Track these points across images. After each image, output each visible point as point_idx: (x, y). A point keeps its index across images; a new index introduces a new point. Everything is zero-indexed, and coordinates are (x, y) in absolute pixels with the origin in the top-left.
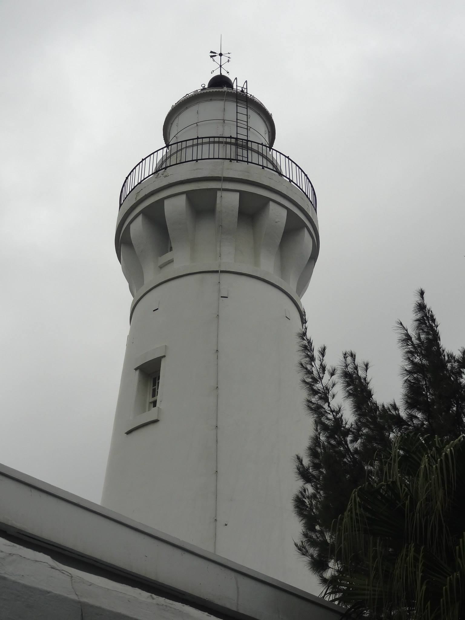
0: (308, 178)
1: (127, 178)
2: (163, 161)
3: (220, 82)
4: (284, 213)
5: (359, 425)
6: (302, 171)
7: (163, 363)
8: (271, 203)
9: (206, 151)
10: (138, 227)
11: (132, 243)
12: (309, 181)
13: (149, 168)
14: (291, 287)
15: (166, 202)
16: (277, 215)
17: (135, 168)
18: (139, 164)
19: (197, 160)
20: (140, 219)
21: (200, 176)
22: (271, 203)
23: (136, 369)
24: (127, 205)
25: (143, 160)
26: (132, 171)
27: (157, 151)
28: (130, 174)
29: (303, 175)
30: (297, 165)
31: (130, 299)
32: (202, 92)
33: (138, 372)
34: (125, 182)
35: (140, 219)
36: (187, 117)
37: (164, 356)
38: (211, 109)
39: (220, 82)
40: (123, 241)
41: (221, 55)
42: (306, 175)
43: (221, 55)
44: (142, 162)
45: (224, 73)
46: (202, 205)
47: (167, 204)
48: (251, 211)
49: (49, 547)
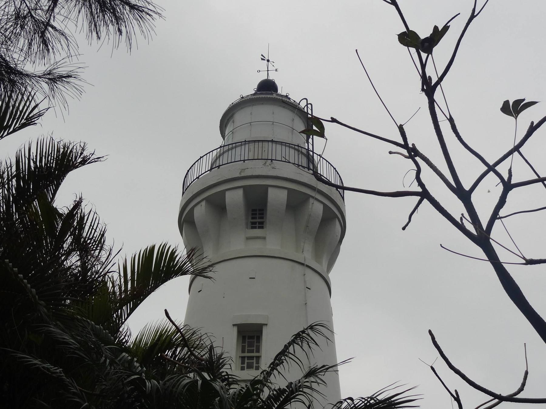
0: (336, 171)
1: (188, 171)
2: (218, 157)
3: (267, 87)
5: (131, 290)
6: (331, 165)
7: (265, 330)
9: (279, 152)
10: (200, 211)
11: (194, 222)
12: (338, 173)
13: (205, 165)
14: (321, 268)
17: (195, 163)
18: (198, 161)
19: (244, 161)
20: (203, 203)
21: (302, 181)
23: (234, 325)
24: (189, 195)
25: (201, 157)
26: (193, 166)
27: (212, 151)
28: (191, 168)
29: (332, 168)
30: (327, 161)
32: (253, 97)
33: (235, 329)
34: (187, 174)
35: (203, 203)
37: (266, 325)
38: (264, 112)
39: (267, 87)
41: (268, 61)
42: (335, 169)
43: (268, 61)
44: (200, 159)
45: (271, 78)
46: (218, 205)
47: (228, 195)
48: (296, 203)
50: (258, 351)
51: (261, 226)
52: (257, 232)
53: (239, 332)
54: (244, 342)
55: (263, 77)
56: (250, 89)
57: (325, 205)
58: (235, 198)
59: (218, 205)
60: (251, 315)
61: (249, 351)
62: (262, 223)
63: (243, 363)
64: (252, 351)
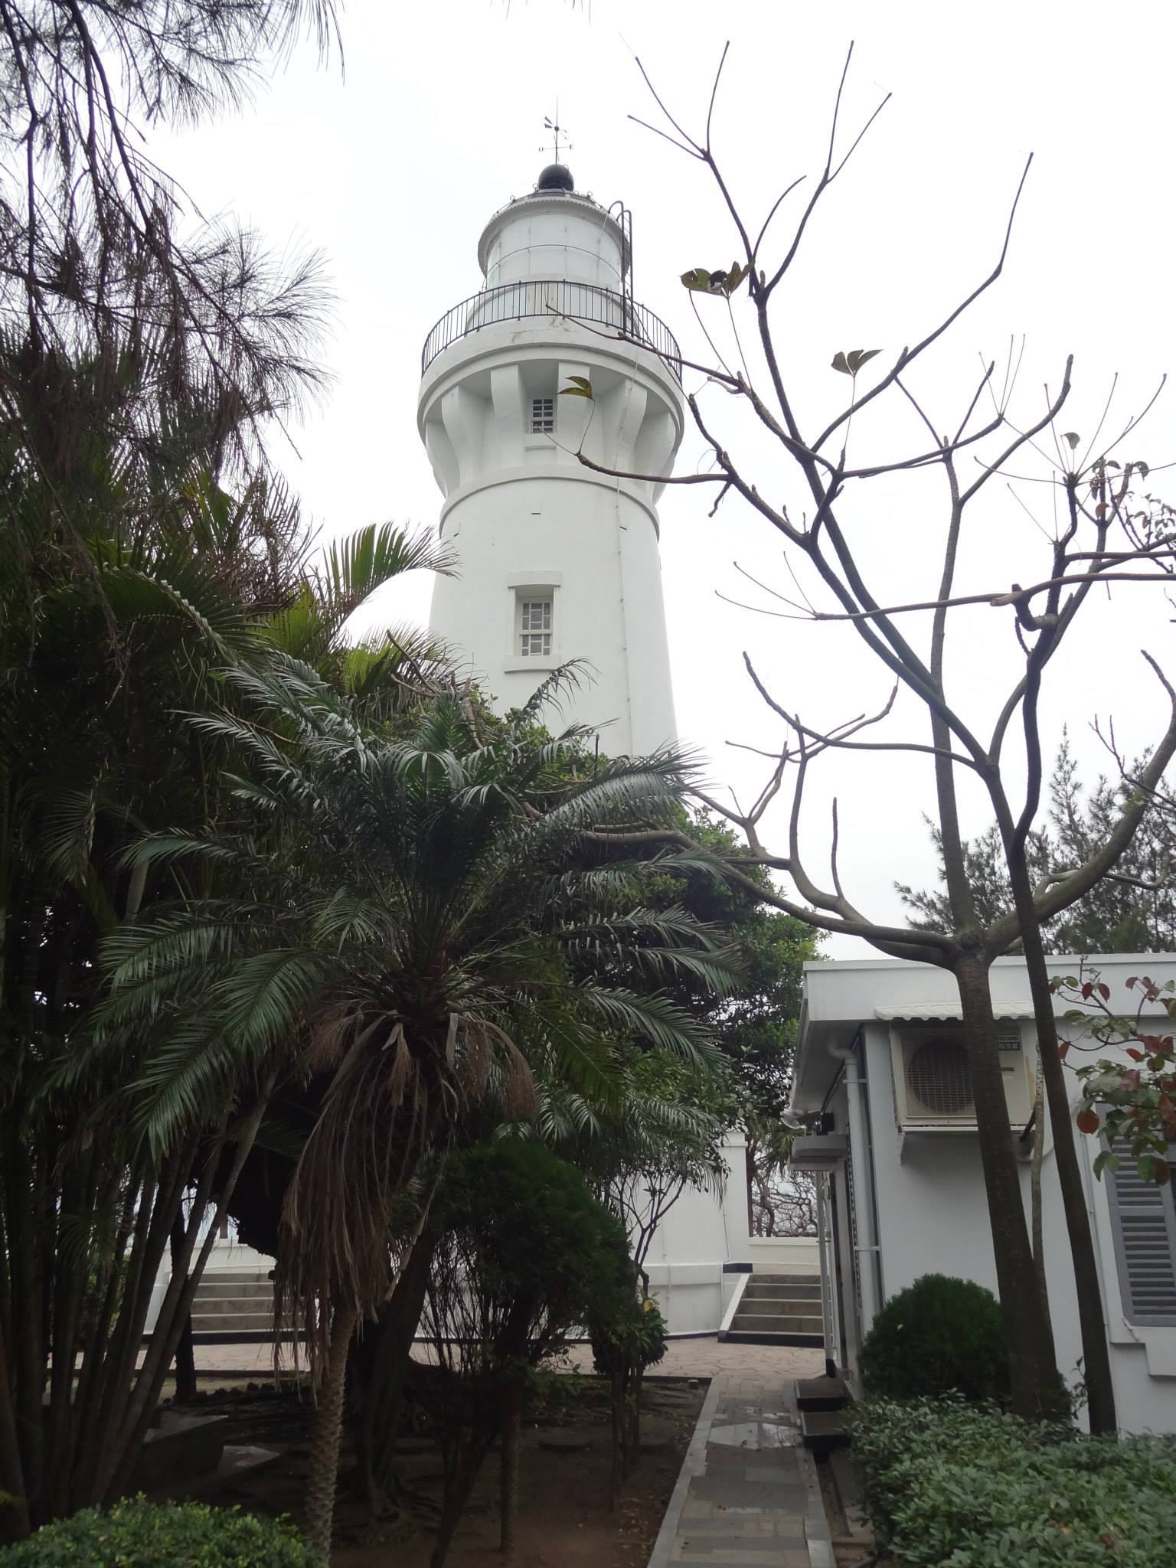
3: (556, 179)
4: (644, 394)
8: (628, 384)
10: (452, 405)
15: (494, 375)
16: (636, 398)
20: (456, 391)
22: (628, 384)
24: (433, 375)
31: (532, 191)
32: (532, 200)
33: (513, 593)
35: (456, 391)
36: (513, 237)
40: (430, 420)
41: (557, 129)
43: (557, 129)
45: (561, 163)
46: (480, 395)
47: (495, 376)
49: (176, 1297)
50: (547, 626)
51: (549, 427)
52: (541, 439)
53: (518, 598)
54: (526, 613)
55: (547, 161)
56: (526, 184)
57: (650, 392)
58: (506, 383)
59: (480, 395)
60: (536, 575)
61: (534, 627)
62: (550, 423)
63: (525, 644)
64: (538, 627)
